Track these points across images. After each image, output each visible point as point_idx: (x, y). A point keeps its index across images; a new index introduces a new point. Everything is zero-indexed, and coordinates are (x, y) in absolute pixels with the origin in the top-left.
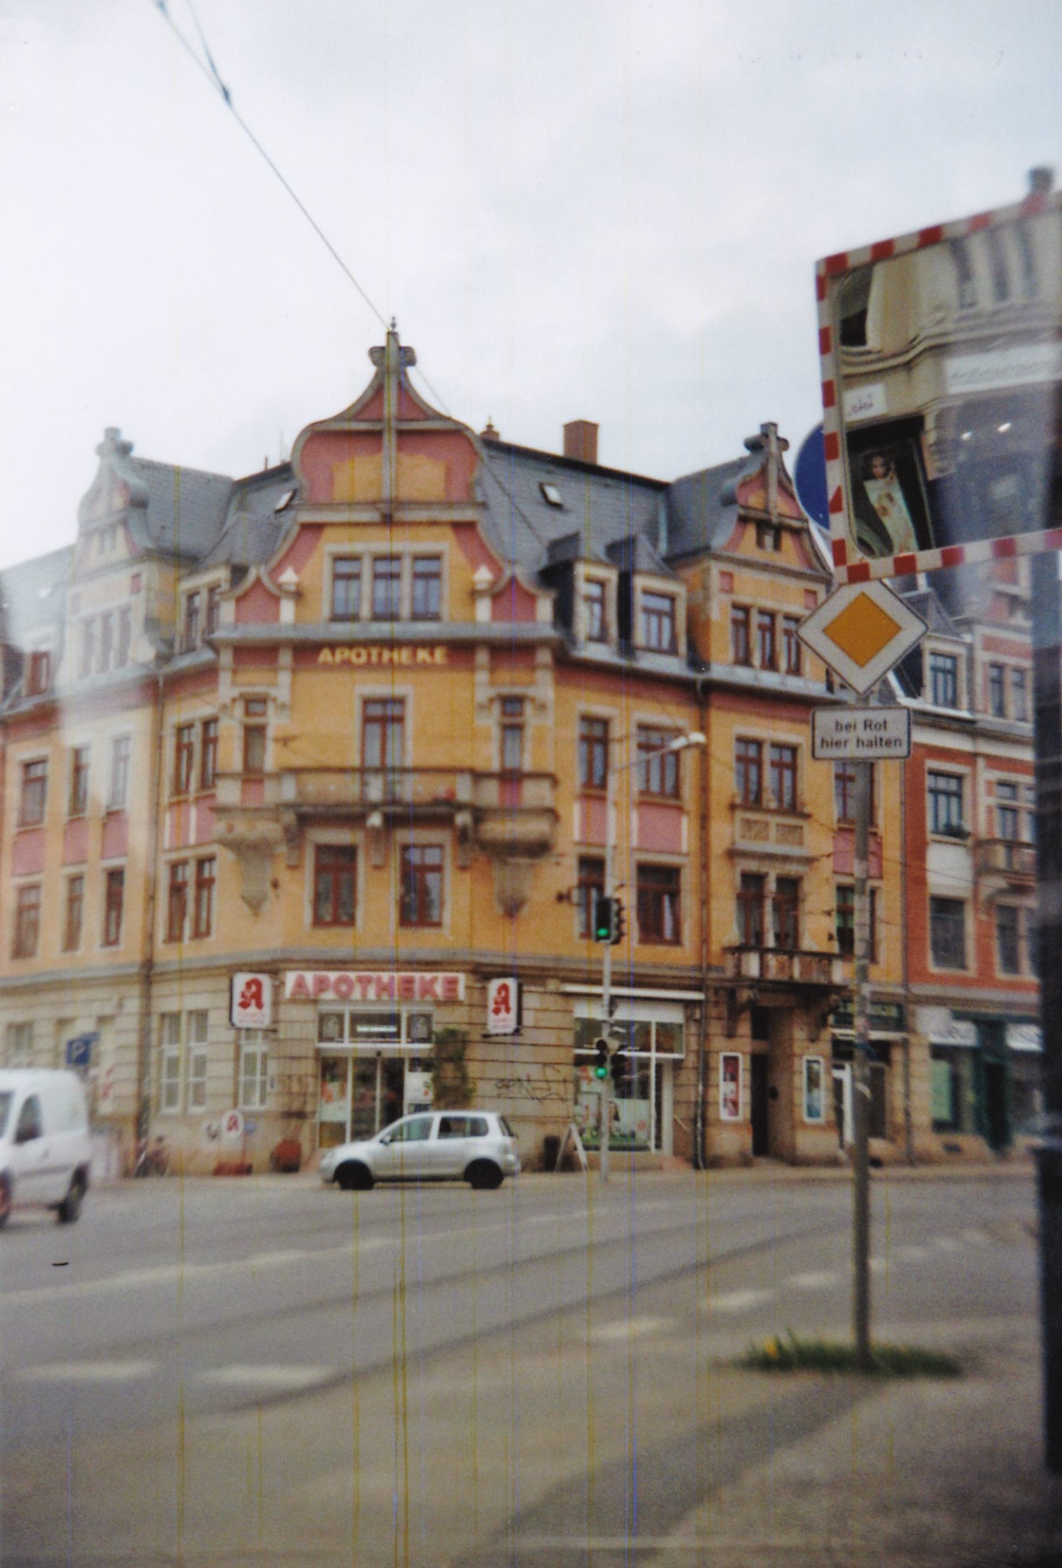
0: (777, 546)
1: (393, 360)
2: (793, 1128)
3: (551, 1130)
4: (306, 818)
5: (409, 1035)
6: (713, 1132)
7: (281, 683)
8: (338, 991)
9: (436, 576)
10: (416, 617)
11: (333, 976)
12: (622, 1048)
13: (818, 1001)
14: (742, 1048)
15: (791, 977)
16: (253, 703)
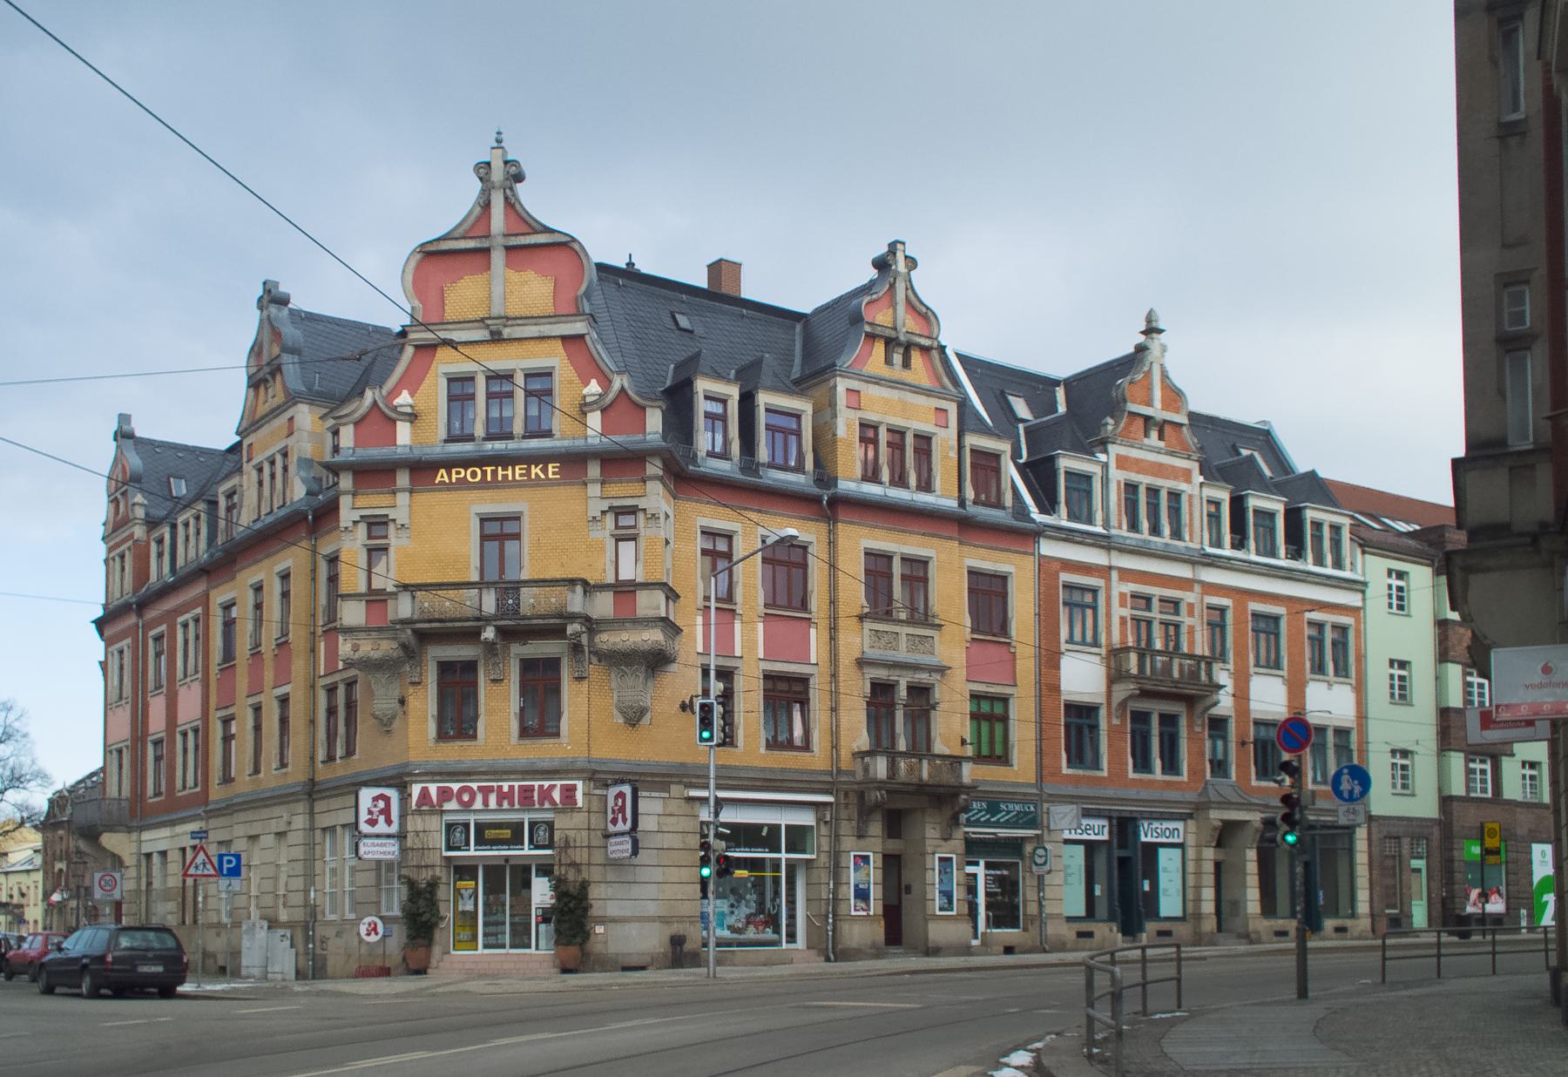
0: (906, 364)
1: (497, 174)
2: (926, 921)
3: (676, 929)
4: (426, 634)
5: (531, 842)
6: (845, 928)
7: (401, 505)
8: (460, 801)
9: (549, 392)
10: (529, 435)
11: (455, 787)
12: (728, 848)
13: (945, 799)
14: (874, 847)
15: (921, 779)
16: (377, 524)
